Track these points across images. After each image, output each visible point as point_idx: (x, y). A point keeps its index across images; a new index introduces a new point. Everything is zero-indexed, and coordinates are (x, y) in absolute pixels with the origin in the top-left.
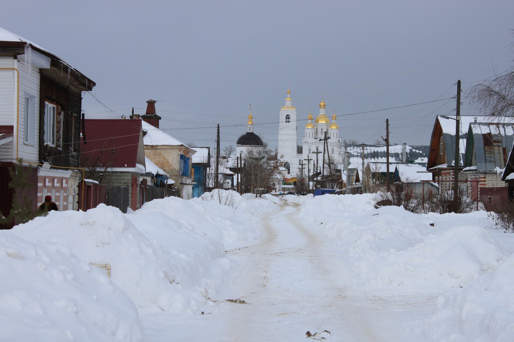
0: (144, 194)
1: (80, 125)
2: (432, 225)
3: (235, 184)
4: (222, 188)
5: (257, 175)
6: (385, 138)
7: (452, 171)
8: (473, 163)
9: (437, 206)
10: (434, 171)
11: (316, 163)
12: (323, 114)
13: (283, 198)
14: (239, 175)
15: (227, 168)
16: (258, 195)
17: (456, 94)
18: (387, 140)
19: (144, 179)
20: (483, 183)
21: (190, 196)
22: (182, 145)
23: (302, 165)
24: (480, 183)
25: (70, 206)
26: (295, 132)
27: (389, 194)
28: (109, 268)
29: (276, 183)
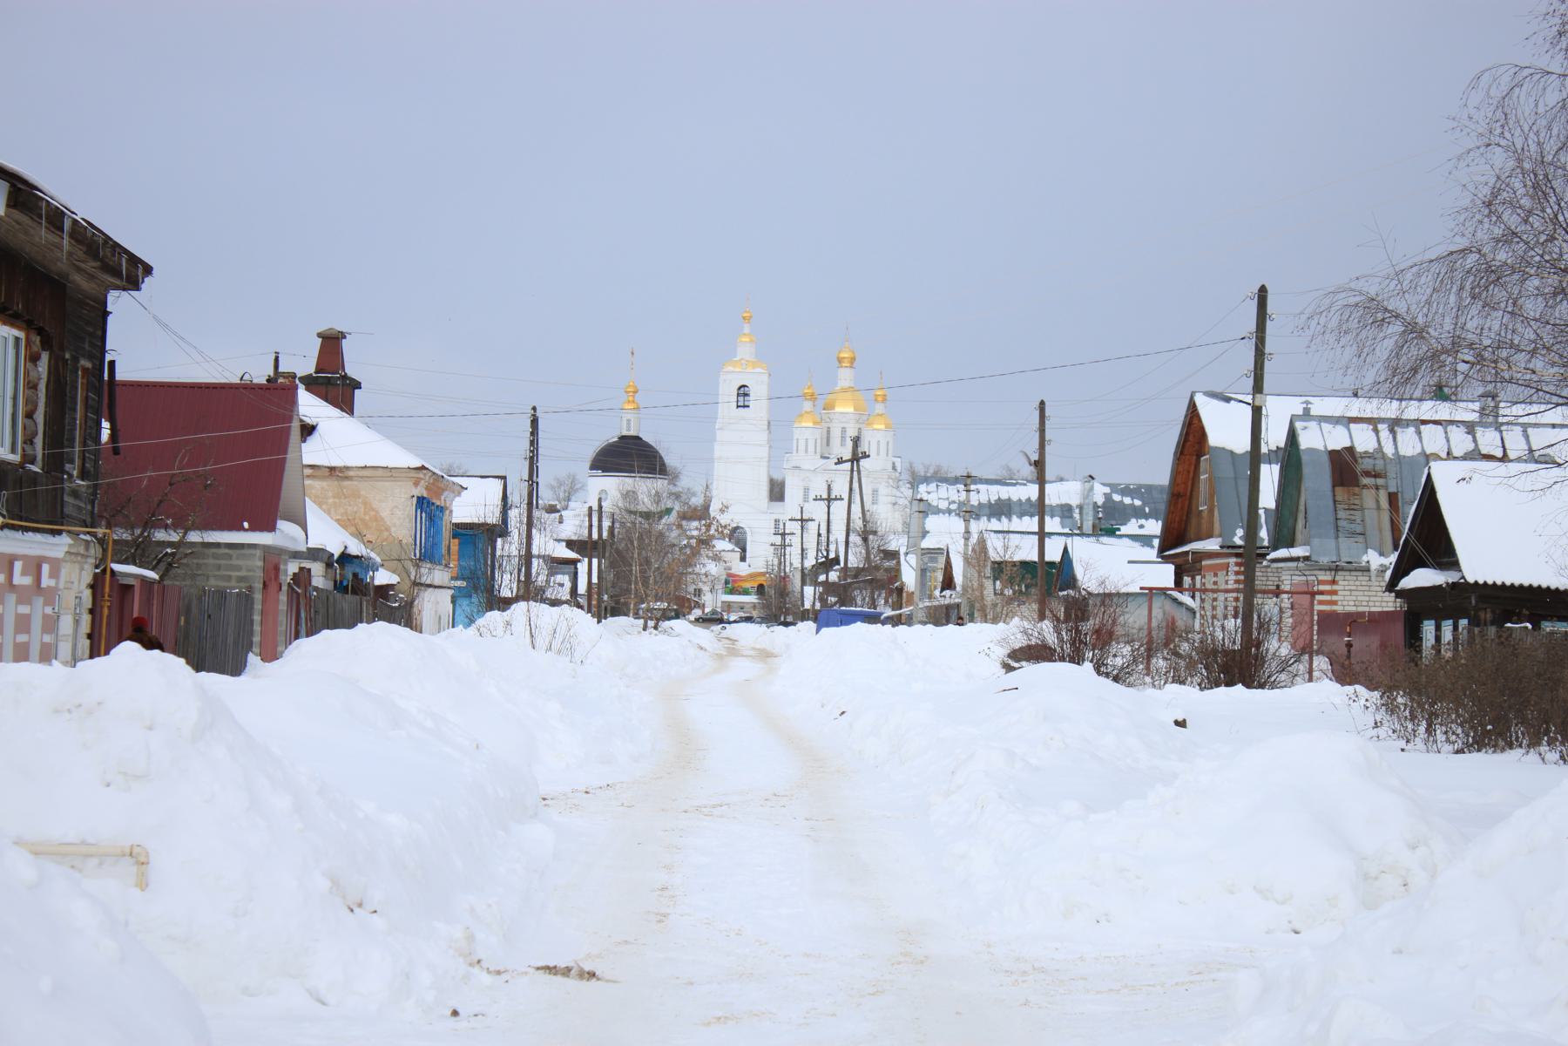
0: (303, 615)
1: (100, 396)
2: (1181, 724)
3: (582, 588)
4: (543, 601)
5: (648, 562)
6: (1035, 457)
7: (1233, 560)
8: (1299, 537)
9: (1191, 666)
10: (1180, 561)
11: (823, 531)
12: (847, 384)
13: (725, 634)
14: (595, 561)
15: (559, 541)
16: (651, 623)
17: (1253, 327)
18: (1039, 465)
19: (301, 569)
20: (1328, 598)
21: (445, 621)
22: (423, 468)
23: (783, 535)
24: (1318, 597)
25: (65, 648)
26: (763, 436)
27: (1047, 626)
28: (143, 859)
29: (706, 588)
